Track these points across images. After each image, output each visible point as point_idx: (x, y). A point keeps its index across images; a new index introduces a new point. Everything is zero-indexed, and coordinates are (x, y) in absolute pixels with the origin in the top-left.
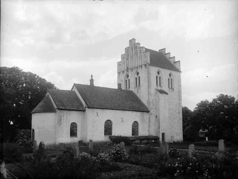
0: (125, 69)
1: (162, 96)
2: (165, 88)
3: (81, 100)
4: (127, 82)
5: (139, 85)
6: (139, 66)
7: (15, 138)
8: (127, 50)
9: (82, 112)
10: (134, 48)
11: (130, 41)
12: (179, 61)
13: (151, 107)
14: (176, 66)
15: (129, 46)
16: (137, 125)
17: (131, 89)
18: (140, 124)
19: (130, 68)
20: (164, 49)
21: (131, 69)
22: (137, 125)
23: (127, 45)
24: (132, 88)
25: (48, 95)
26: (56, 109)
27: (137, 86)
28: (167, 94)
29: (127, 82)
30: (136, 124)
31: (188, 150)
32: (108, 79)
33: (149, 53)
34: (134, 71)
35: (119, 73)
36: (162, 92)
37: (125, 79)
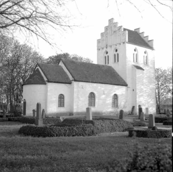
0: (103, 45)
1: (138, 71)
2: (141, 64)
3: (68, 75)
4: (107, 59)
5: (118, 61)
6: (118, 44)
7: (95, 118)
8: (106, 28)
9: (67, 85)
10: (112, 28)
11: (109, 20)
12: (152, 40)
13: (128, 81)
14: (150, 44)
15: (109, 24)
16: (116, 98)
17: (109, 65)
18: (95, 93)
19: (109, 45)
20: (112, 19)
21: (110, 46)
22: (116, 98)
23: (107, 24)
24: (111, 64)
25: (38, 69)
26: (47, 81)
27: (115, 62)
28: (143, 70)
29: (107, 59)
30: (92, 95)
31: (3, 106)
32: (91, 55)
33: (127, 32)
34: (113, 48)
35: (99, 49)
36: (139, 68)
37: (104, 55)
